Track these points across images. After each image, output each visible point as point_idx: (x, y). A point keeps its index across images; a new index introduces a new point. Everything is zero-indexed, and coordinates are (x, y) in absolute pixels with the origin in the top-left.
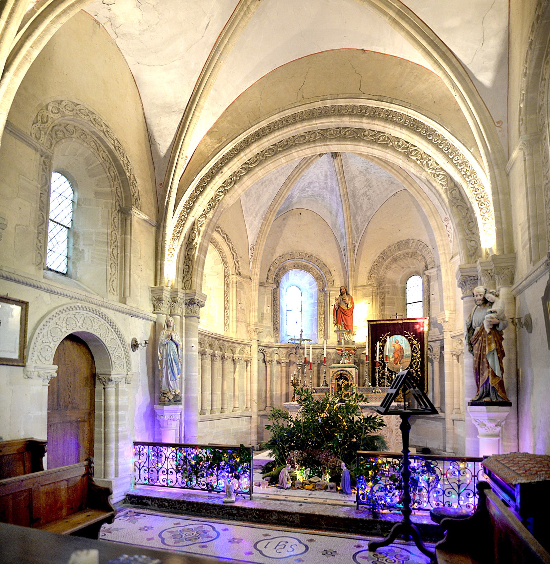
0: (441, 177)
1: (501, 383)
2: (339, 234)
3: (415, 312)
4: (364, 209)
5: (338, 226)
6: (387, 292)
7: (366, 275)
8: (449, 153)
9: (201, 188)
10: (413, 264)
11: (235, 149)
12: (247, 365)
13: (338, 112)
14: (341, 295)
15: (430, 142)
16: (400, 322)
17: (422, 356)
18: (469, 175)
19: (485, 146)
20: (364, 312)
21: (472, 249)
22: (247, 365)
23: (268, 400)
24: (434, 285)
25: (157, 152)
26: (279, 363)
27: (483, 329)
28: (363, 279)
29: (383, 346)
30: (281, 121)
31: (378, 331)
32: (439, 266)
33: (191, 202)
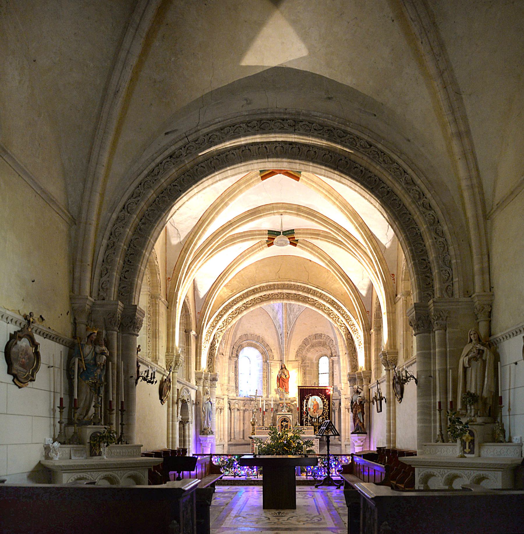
0: (343, 327)
1: (363, 425)
2: (278, 325)
3: (324, 381)
4: (295, 311)
5: (277, 319)
6: (308, 368)
7: (295, 354)
8: (348, 319)
9: (221, 315)
10: (324, 350)
11: (240, 296)
12: (221, 412)
13: (297, 288)
14: (282, 369)
15: (340, 312)
16: (317, 388)
17: (329, 408)
18: (355, 331)
19: (362, 322)
20: (295, 381)
21: (354, 366)
22: (221, 412)
23: (232, 434)
24: (336, 366)
25: (198, 295)
26: (238, 410)
27: (356, 403)
28: (292, 357)
29: (307, 402)
30: (267, 286)
31: (304, 393)
32: (339, 356)
33: (214, 323)
